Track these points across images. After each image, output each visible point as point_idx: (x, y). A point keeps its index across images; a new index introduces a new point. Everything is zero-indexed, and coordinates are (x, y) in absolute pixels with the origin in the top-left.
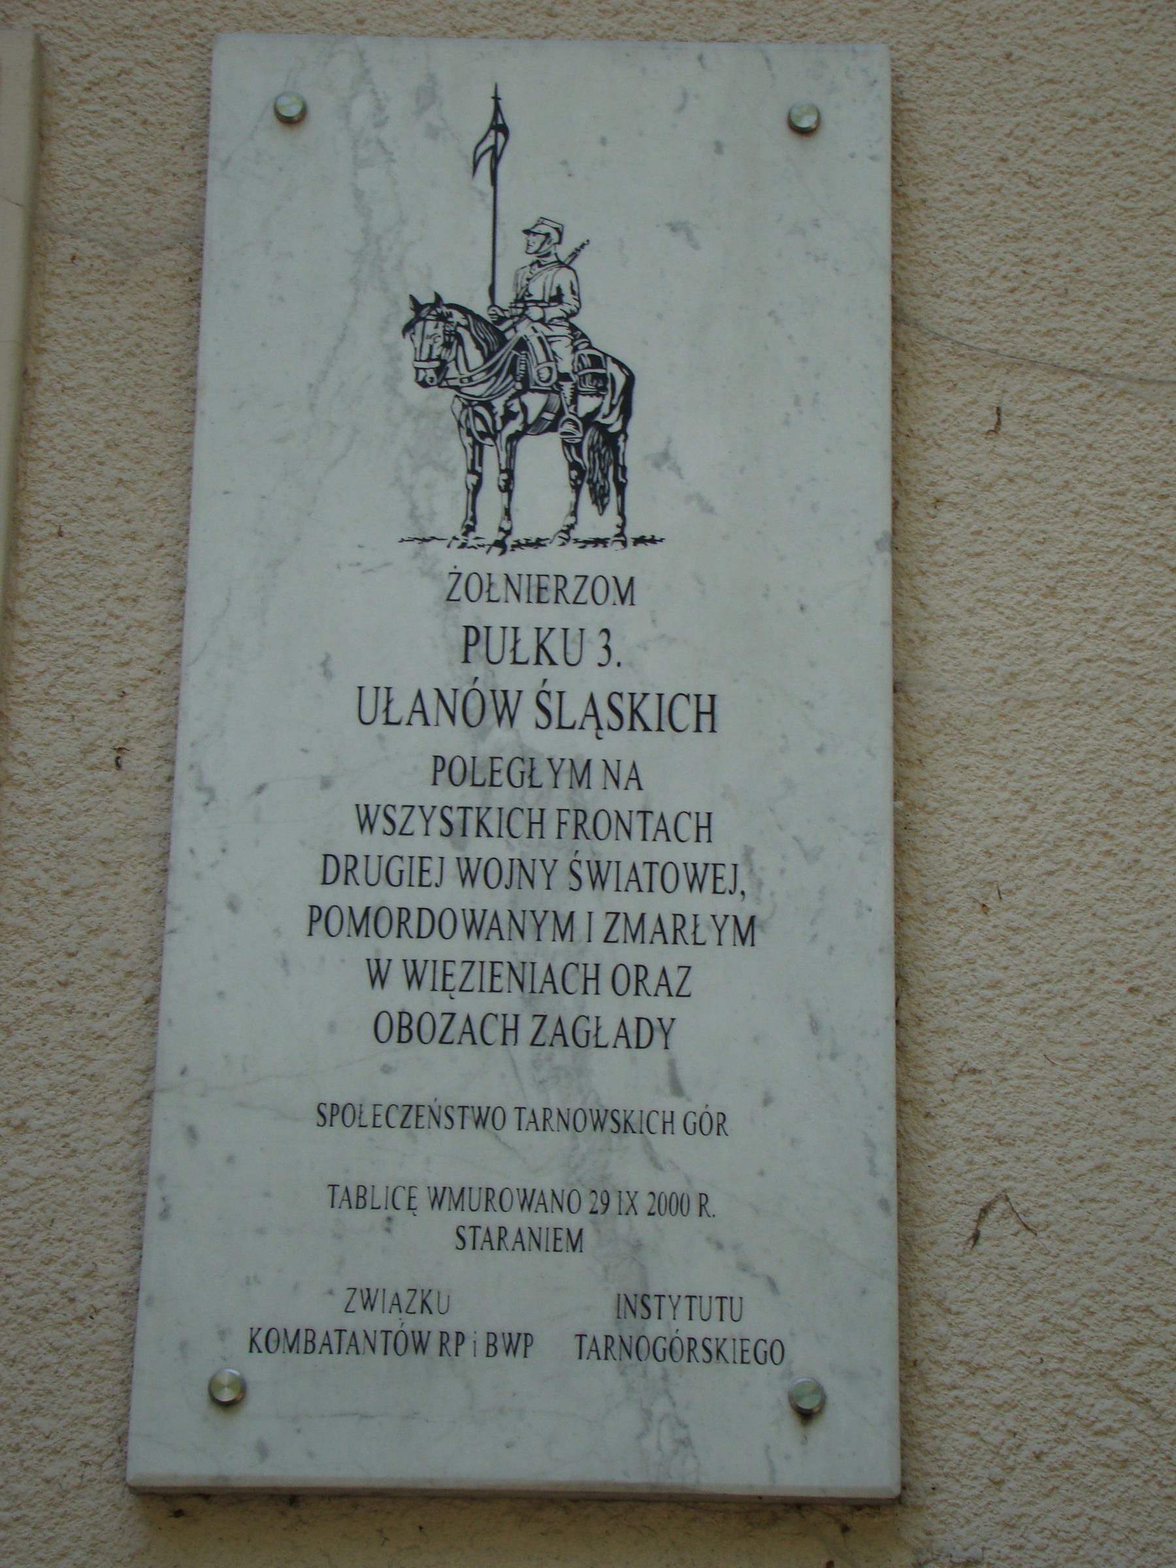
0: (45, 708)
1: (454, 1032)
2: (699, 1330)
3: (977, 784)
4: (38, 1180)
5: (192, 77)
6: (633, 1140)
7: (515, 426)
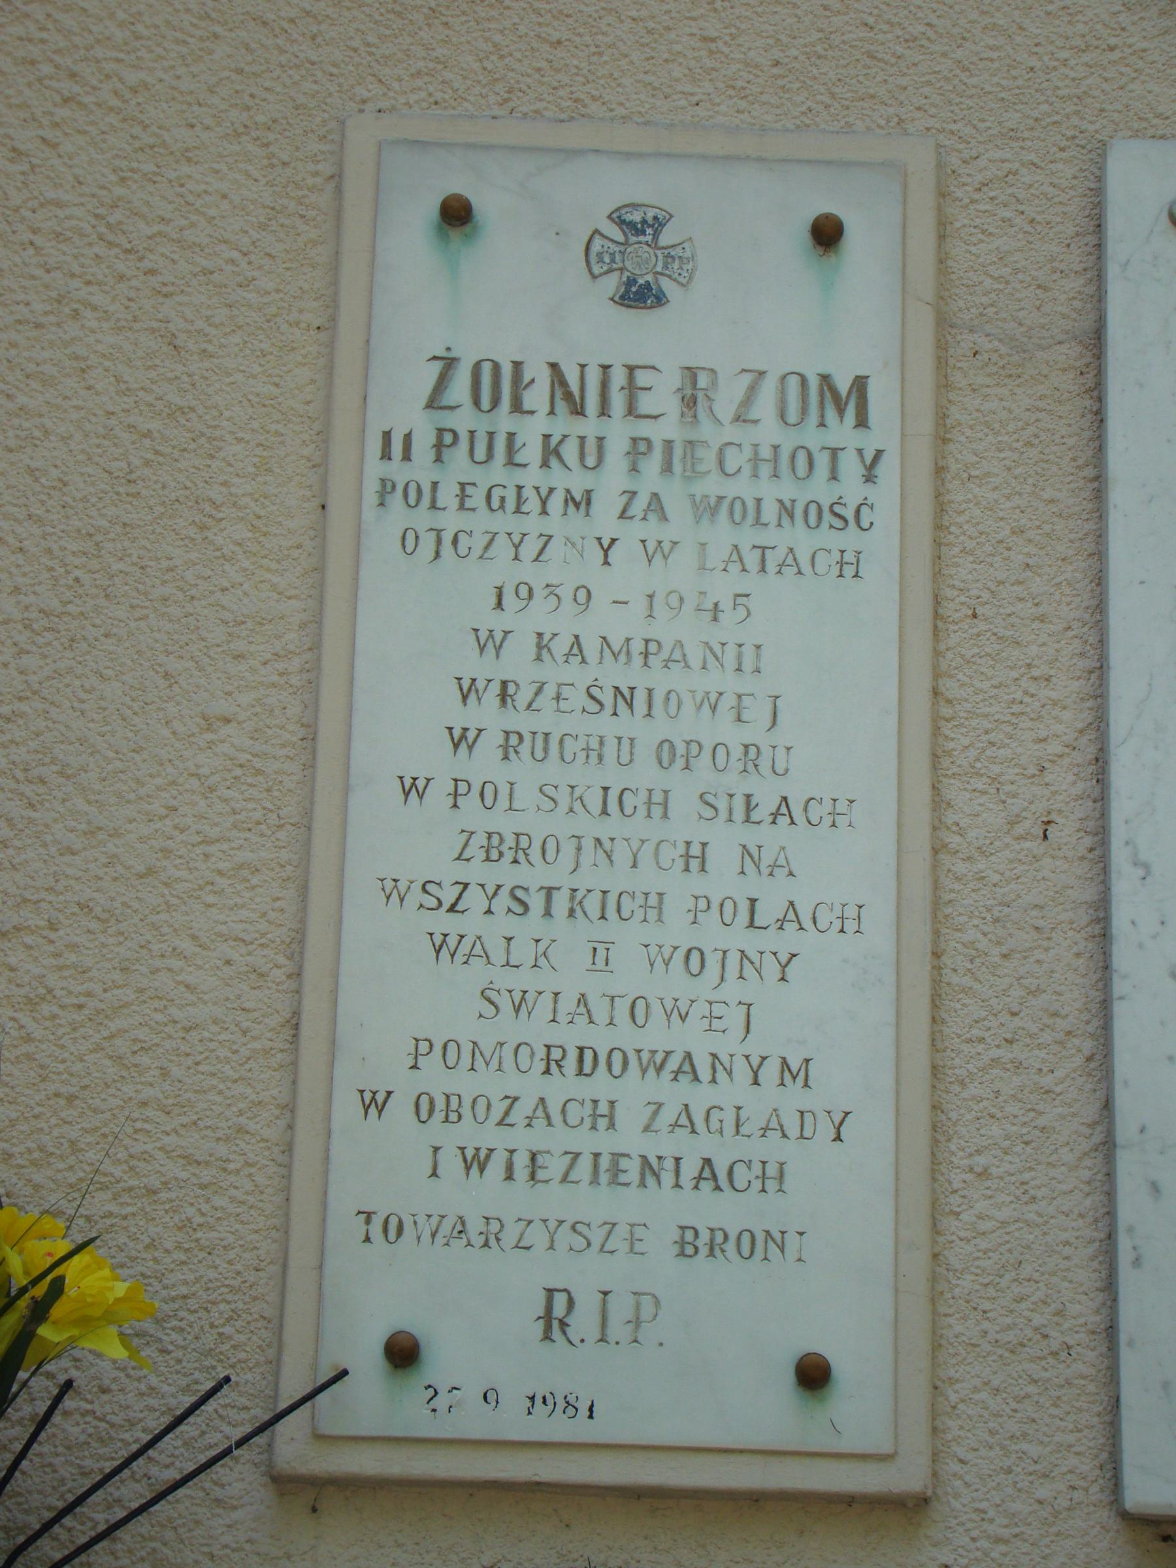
0: (972, 781)
4: (1004, 1224)
5: (1075, 178)
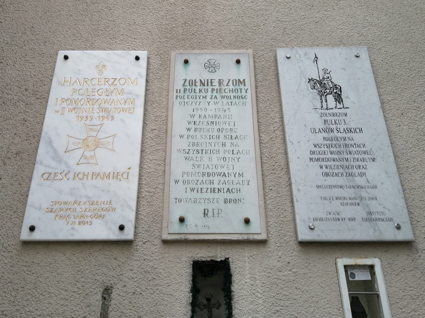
1: (334, 175)
2: (380, 217)
3: (398, 140)
6: (364, 190)
7: (326, 94)
